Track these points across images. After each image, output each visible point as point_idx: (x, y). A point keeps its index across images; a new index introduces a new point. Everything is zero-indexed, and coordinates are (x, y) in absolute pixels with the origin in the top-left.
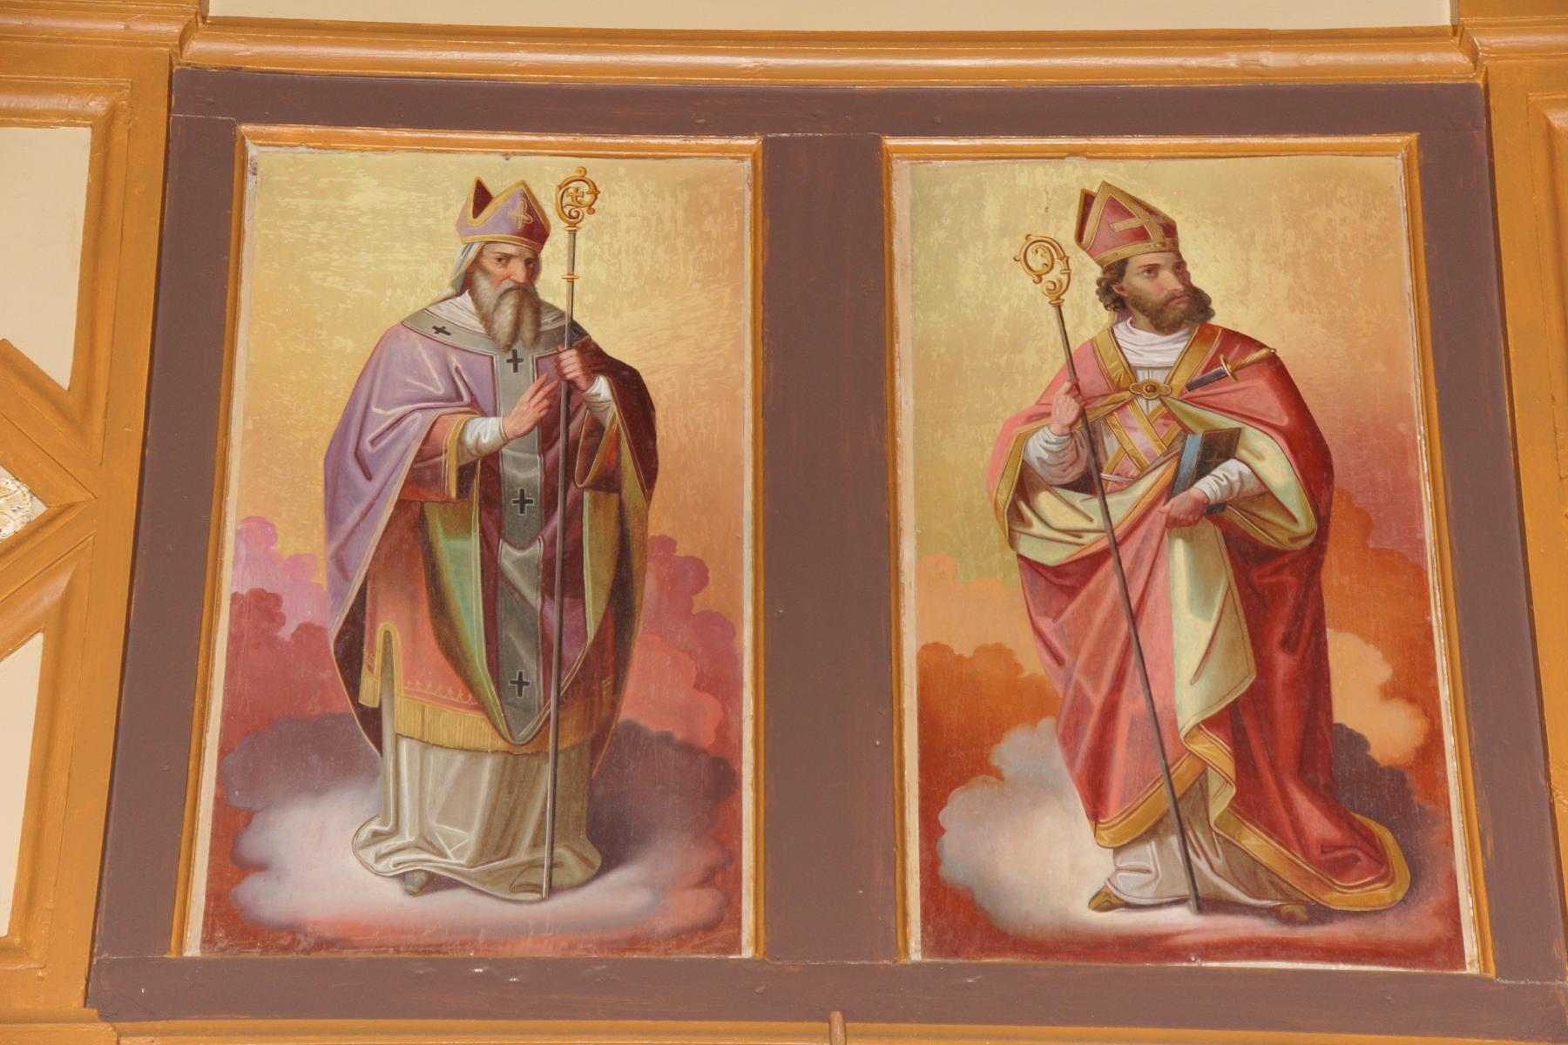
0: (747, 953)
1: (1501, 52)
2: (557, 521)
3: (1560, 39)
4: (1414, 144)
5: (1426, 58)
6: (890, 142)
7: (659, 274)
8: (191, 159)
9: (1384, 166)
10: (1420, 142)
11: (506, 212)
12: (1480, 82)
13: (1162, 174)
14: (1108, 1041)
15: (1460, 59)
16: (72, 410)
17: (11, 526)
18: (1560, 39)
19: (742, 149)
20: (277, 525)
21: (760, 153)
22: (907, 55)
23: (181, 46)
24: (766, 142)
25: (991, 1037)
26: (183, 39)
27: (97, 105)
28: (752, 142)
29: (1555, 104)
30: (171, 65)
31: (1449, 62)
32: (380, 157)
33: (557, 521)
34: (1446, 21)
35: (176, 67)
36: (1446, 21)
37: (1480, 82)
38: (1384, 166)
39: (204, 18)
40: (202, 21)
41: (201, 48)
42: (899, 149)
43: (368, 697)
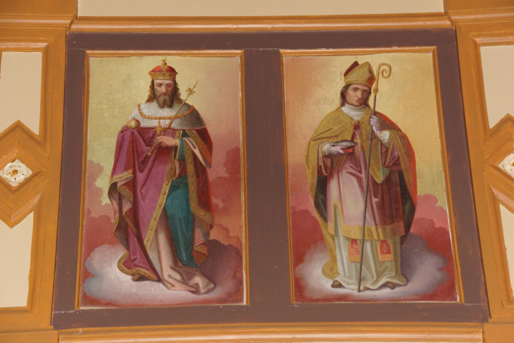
0: (245, 303)
4: (436, 49)
5: (429, 23)
6: (88, 52)
8: (74, 59)
9: (424, 58)
11: (357, 76)
12: (454, 28)
15: (448, 23)
19: (237, 54)
20: (101, 151)
21: (243, 55)
22: (141, 24)
23: (70, 27)
24: (245, 52)
26: (71, 24)
29: (478, 36)
31: (446, 23)
36: (442, 10)
37: (454, 28)
38: (424, 58)
39: (77, 17)
40: (76, 19)
41: (74, 27)
42: (91, 54)
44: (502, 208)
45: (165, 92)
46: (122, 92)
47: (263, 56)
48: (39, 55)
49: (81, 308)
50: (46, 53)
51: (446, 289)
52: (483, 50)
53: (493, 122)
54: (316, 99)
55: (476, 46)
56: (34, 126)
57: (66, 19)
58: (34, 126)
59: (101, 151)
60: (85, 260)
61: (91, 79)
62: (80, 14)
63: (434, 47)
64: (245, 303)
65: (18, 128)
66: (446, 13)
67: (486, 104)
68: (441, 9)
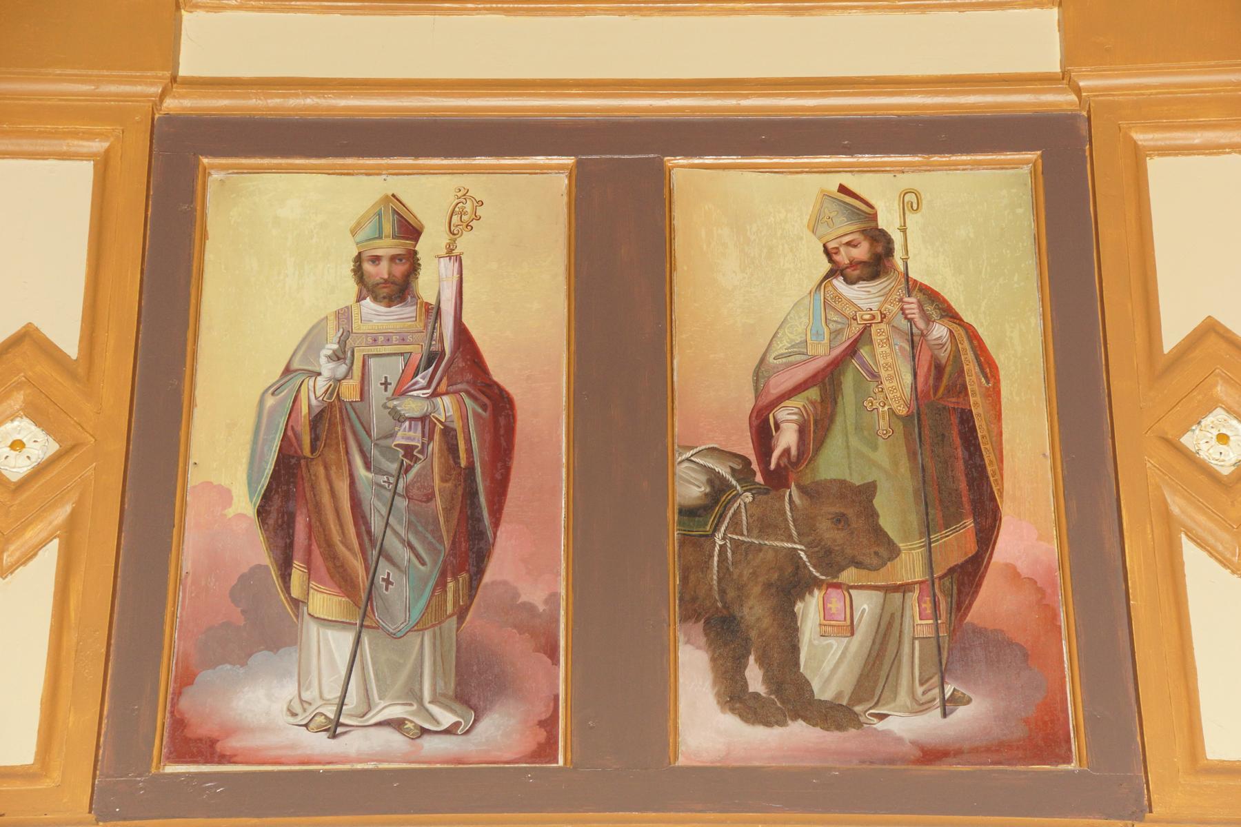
1: (1089, 89)
2: (431, 369)
3: (1233, 78)
7: (508, 272)
10: (1042, 156)
13: (881, 185)
14: (850, 824)
15: (1073, 98)
16: (81, 372)
17: (18, 467)
18: (1233, 78)
20: (224, 462)
24: (579, 164)
25: (764, 822)
27: (98, 146)
28: (569, 161)
30: (153, 114)
31: (1062, 100)
32: (581, 19)
33: (431, 369)
34: (1056, 68)
35: (157, 116)
36: (1056, 68)
39: (174, 79)
41: (172, 104)
42: (213, 167)
43: (296, 592)
44: (1190, 551)
45: (386, 276)
46: (282, 270)
47: (621, 180)
48: (86, 170)
49: (171, 769)
50: (103, 167)
51: (1046, 739)
52: (1156, 167)
53: (1172, 336)
54: (751, 268)
55: (1138, 156)
56: (67, 336)
57: (152, 84)
58: (67, 336)
59: (224, 462)
60: (178, 694)
61: (197, 412)
62: (183, 72)
63: (1032, 156)
64: (561, 762)
65: (28, 338)
66: (1065, 75)
67: (1200, 720)
68: (1054, 66)
